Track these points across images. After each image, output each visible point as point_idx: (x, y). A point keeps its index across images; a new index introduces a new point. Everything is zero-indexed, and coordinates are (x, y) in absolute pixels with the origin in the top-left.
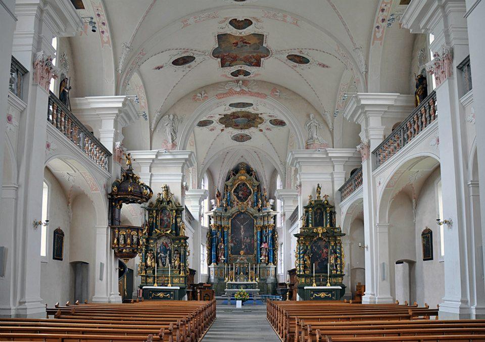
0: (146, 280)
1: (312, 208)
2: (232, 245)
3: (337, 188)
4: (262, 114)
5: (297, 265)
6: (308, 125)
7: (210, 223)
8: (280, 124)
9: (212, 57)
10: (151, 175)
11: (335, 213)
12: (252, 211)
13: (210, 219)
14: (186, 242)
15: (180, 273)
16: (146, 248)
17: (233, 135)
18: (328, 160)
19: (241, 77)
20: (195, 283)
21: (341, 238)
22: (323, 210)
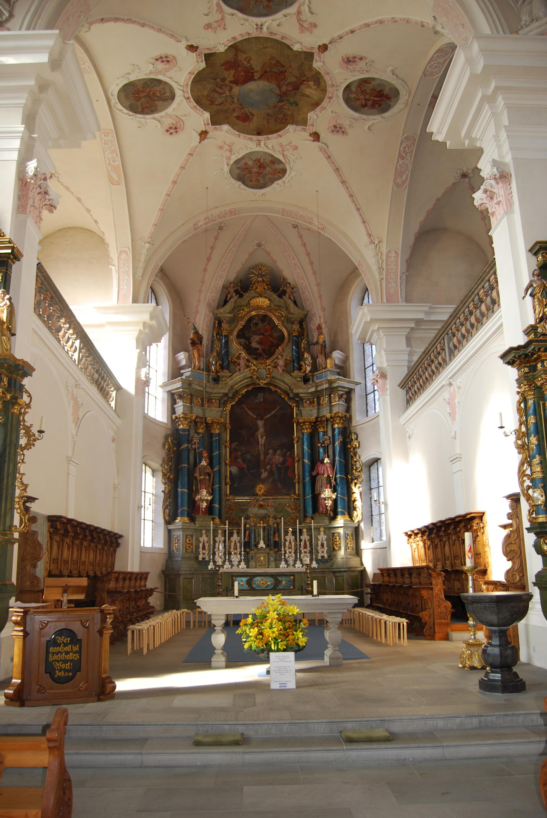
2: (234, 470)
7: (173, 411)
8: (373, 106)
12: (288, 381)
17: (234, 158)
20: (117, 568)
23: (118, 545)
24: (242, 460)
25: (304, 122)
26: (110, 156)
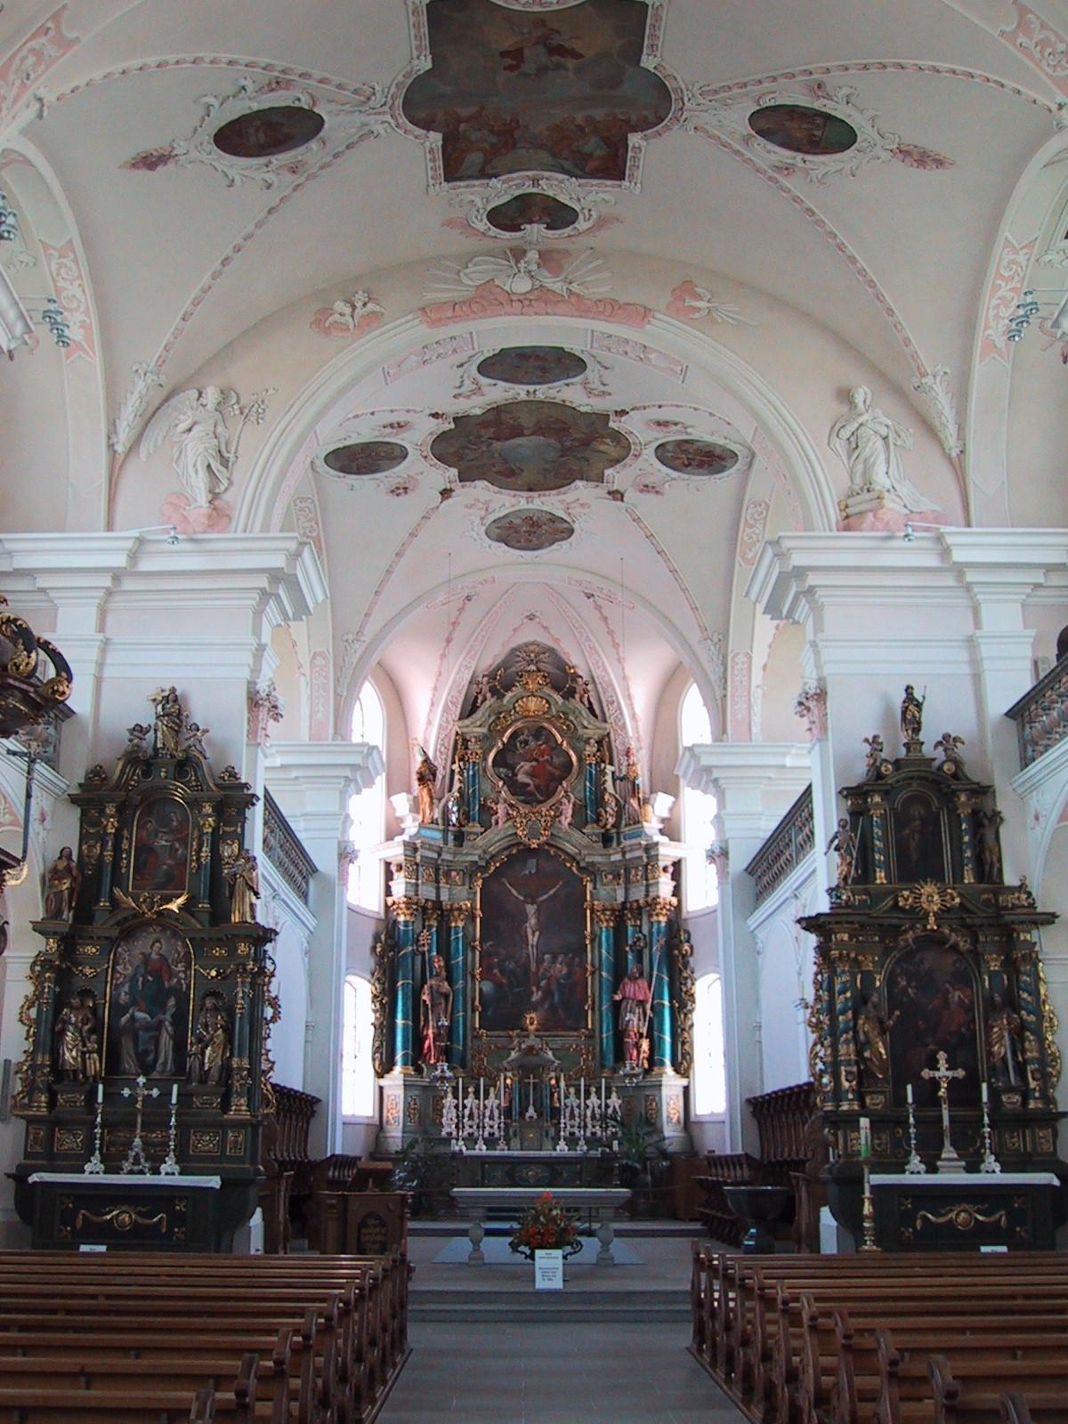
0: (51, 1137)
1: (886, 794)
3: (1002, 699)
4: (623, 413)
5: (820, 1066)
6: (845, 433)
7: (388, 892)
8: (701, 465)
9: (403, 120)
10: (106, 645)
11: (996, 818)
12: (575, 842)
13: (389, 876)
14: (260, 957)
15: (225, 1107)
16: (58, 982)
17: (492, 517)
18: (950, 580)
19: (535, 231)
21: (1033, 936)
22: (936, 804)
23: (313, 1113)
24: (501, 971)
25: (601, 479)
26: (306, 525)
